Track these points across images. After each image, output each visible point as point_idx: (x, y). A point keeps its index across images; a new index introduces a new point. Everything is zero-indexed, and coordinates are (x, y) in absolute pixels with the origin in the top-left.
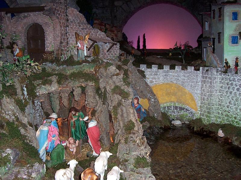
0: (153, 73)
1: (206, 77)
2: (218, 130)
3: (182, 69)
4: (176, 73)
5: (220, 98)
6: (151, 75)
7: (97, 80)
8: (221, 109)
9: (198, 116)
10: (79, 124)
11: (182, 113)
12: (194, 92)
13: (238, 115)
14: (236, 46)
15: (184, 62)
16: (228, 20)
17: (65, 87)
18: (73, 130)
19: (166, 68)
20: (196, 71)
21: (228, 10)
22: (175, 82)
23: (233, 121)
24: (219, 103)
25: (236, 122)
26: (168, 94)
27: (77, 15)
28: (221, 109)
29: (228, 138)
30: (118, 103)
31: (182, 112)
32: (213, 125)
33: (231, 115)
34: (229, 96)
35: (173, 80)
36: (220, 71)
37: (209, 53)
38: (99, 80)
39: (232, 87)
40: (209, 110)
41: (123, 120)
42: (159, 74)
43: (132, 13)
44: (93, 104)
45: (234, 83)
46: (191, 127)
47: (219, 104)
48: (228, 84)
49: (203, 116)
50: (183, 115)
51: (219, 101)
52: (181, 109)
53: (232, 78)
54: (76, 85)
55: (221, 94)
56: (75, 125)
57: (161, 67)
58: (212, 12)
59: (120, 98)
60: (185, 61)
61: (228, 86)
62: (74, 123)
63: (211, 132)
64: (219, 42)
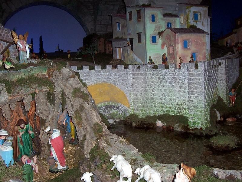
0: (85, 74)
1: (138, 74)
2: (156, 121)
3: (102, 69)
4: (107, 72)
5: (152, 92)
6: (83, 76)
7: (51, 85)
8: (154, 102)
9: (130, 112)
10: (25, 139)
11: (112, 112)
12: (125, 89)
14: (155, 44)
15: (95, 62)
16: (149, 22)
17: (16, 96)
18: (21, 146)
19: (98, 68)
20: (125, 69)
21: (148, 12)
22: (107, 82)
24: (152, 97)
25: (172, 111)
26: (101, 94)
28: (154, 102)
29: (170, 126)
30: (80, 107)
31: (113, 111)
32: (149, 117)
33: (165, 106)
34: (162, 89)
35: (105, 79)
36: (150, 67)
37: (129, 52)
38: (54, 83)
39: (164, 81)
40: (144, 105)
41: (90, 125)
42: (91, 74)
43: (12, 14)
44: (47, 112)
45: (166, 77)
46: (128, 123)
47: (151, 98)
48: (159, 79)
49: (137, 110)
50: (114, 113)
51: (151, 95)
52: (112, 107)
53: (163, 72)
54: (25, 93)
56: (21, 140)
57: (92, 68)
58: (128, 14)
59: (81, 100)
60: (95, 62)
61: (159, 81)
62: (21, 137)
63: (150, 124)
64: (140, 41)
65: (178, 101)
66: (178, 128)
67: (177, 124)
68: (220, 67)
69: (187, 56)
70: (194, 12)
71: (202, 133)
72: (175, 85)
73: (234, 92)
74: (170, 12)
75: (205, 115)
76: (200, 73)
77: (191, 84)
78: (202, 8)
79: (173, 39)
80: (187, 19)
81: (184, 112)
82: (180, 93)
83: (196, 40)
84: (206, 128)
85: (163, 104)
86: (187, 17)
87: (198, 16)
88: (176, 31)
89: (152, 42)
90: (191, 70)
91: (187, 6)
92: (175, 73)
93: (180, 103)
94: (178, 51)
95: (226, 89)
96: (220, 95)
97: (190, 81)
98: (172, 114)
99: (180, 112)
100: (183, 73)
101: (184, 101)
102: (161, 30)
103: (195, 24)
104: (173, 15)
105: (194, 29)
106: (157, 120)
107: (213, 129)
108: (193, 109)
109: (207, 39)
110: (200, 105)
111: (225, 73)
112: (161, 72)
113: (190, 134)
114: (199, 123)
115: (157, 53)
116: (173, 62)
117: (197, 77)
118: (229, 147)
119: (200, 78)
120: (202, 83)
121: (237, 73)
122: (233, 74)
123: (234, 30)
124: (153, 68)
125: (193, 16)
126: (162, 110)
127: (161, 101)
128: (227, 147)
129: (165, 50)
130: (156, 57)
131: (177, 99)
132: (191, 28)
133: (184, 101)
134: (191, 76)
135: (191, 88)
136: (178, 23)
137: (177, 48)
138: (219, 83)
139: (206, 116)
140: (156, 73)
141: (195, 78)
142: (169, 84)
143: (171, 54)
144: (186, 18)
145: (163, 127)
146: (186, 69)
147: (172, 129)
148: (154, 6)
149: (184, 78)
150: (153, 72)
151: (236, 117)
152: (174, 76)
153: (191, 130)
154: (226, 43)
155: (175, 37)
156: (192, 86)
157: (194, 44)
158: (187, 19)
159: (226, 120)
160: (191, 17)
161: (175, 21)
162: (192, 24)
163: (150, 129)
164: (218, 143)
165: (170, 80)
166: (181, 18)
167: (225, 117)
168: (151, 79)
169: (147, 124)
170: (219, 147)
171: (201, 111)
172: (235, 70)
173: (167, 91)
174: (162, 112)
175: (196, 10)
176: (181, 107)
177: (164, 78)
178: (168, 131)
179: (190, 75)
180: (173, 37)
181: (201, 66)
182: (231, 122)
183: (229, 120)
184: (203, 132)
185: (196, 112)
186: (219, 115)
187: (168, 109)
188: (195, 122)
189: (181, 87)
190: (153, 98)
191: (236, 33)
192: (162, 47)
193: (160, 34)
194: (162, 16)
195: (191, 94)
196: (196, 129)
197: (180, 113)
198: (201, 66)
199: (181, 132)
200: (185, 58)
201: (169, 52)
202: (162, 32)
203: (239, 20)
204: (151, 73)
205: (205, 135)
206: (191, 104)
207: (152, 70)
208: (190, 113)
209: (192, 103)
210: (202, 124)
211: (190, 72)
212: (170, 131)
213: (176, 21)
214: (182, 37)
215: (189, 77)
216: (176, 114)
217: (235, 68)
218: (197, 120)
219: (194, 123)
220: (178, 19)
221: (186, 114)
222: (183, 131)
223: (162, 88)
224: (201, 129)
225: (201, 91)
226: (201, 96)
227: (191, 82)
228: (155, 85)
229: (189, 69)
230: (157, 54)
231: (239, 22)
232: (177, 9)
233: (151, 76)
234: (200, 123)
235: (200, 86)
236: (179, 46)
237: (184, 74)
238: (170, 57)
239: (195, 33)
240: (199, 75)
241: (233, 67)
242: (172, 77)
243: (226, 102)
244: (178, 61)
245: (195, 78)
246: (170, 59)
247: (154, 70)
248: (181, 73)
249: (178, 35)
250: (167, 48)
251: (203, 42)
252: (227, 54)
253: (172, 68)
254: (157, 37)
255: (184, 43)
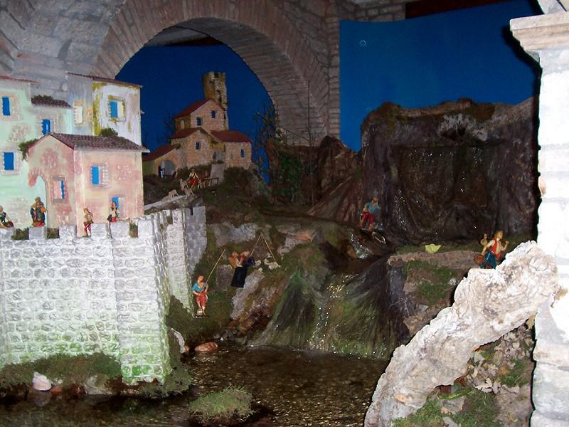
8: (20, 328)
13: (74, 330)
14: (13, 175)
23: (61, 347)
24: (12, 313)
27: (232, 145)
28: (20, 328)
33: (54, 334)
34: (41, 292)
45: (52, 259)
51: (12, 310)
55: (13, 291)
61: (33, 270)
65: (87, 320)
66: (95, 387)
67: (92, 378)
68: (169, 227)
69: (101, 205)
70: (111, 97)
71: (159, 392)
72: (77, 279)
73: (203, 283)
74: (49, 93)
75: (162, 344)
76: (143, 245)
77: (123, 276)
78: (127, 88)
79: (65, 162)
80: (95, 113)
81: (105, 346)
82: (91, 298)
83: (118, 167)
84: (169, 378)
85: (47, 330)
86: (94, 109)
87: (118, 108)
88: (73, 142)
89: (5, 169)
90: (121, 239)
91: (94, 82)
92: (77, 249)
93: (92, 323)
94: (78, 194)
95: (187, 278)
96: (175, 292)
97: (119, 268)
98: (74, 353)
99: (95, 346)
100: (98, 248)
101: (103, 317)
102: (28, 138)
103: (112, 126)
104: (57, 101)
105: (109, 139)
106: (36, 374)
107: (183, 378)
108: (132, 335)
109: (134, 163)
110: (148, 324)
111: (183, 241)
112: (38, 246)
113: (129, 399)
114: (148, 368)
115: (19, 196)
116: (64, 219)
117: (135, 257)
118: (238, 416)
119: (145, 258)
120: (151, 270)
121: (203, 238)
122: (195, 241)
123: (174, 142)
124: (15, 238)
125: (107, 106)
126: (44, 347)
127: (39, 323)
128: (235, 416)
129: (40, 190)
130: (14, 207)
131: (84, 313)
132: (104, 137)
133: (103, 317)
134: (122, 256)
135: (122, 285)
136: (72, 120)
137: (75, 185)
138: (170, 265)
139: (163, 349)
140: (22, 249)
141: (132, 260)
142: (60, 277)
143: (60, 201)
144: (92, 112)
145: (53, 390)
146: (103, 238)
147: (80, 393)
148: (9, 75)
149: (100, 259)
150: (14, 247)
151: (213, 340)
152: (74, 257)
153: (127, 388)
154: (157, 170)
155: (70, 158)
156: (125, 280)
157: (114, 175)
158: (95, 113)
159: (196, 349)
160: (104, 110)
161: (61, 117)
162: (106, 127)
163: (19, 401)
164: (213, 413)
165: (62, 267)
166: (77, 110)
167: (192, 344)
168: (9, 266)
169: (9, 389)
170: (217, 421)
171: (153, 338)
172: (199, 233)
173: (57, 296)
174: (45, 351)
175: (113, 94)
176: (98, 332)
177: (46, 263)
178: (71, 397)
179: (118, 252)
180: (63, 157)
181: (145, 230)
182: (209, 354)
183: (202, 349)
184: (162, 388)
185: (138, 343)
186: (182, 342)
187: (62, 341)
188: (139, 367)
189: (93, 283)
190: (19, 318)
191: (178, 147)
192: (30, 182)
193: (26, 147)
194: (30, 103)
195: (124, 299)
196: (142, 383)
197: (93, 349)
198: (145, 230)
199: (105, 397)
200: (95, 209)
201: (54, 194)
202: (32, 143)
203: (182, 120)
204: (9, 250)
205: (167, 395)
206: (125, 323)
207: (10, 243)
208: (125, 347)
209: (127, 321)
210: (156, 371)
211: (119, 244)
212: (76, 397)
213: (64, 116)
214: (88, 158)
215: (117, 258)
216: (84, 352)
217: (198, 228)
218: (144, 360)
219: (136, 370)
220: (69, 111)
221: (111, 348)
222: (110, 393)
223: (41, 289)
224: (156, 381)
225: (147, 291)
226: (148, 302)
227: (122, 270)
228: (23, 280)
229: (116, 239)
230: (18, 199)
231: (182, 122)
232: (65, 88)
233: (9, 258)
234: (150, 368)
235: (146, 279)
236: (83, 180)
237: (99, 250)
238: (54, 207)
239: (101, 149)
240: (143, 251)
241: (193, 227)
242: (67, 259)
243: (189, 307)
244: (80, 220)
245: (132, 260)
246: (57, 212)
247: (17, 242)
248: (91, 247)
249: (77, 154)
250: (46, 184)
251: (135, 169)
252: (167, 195)
253: (66, 235)
254: (18, 155)
255: (92, 173)
